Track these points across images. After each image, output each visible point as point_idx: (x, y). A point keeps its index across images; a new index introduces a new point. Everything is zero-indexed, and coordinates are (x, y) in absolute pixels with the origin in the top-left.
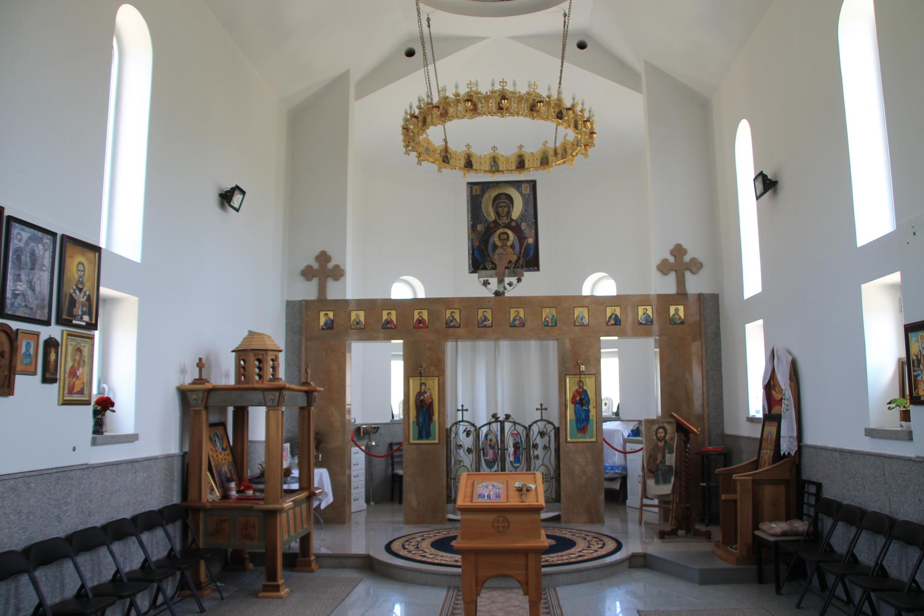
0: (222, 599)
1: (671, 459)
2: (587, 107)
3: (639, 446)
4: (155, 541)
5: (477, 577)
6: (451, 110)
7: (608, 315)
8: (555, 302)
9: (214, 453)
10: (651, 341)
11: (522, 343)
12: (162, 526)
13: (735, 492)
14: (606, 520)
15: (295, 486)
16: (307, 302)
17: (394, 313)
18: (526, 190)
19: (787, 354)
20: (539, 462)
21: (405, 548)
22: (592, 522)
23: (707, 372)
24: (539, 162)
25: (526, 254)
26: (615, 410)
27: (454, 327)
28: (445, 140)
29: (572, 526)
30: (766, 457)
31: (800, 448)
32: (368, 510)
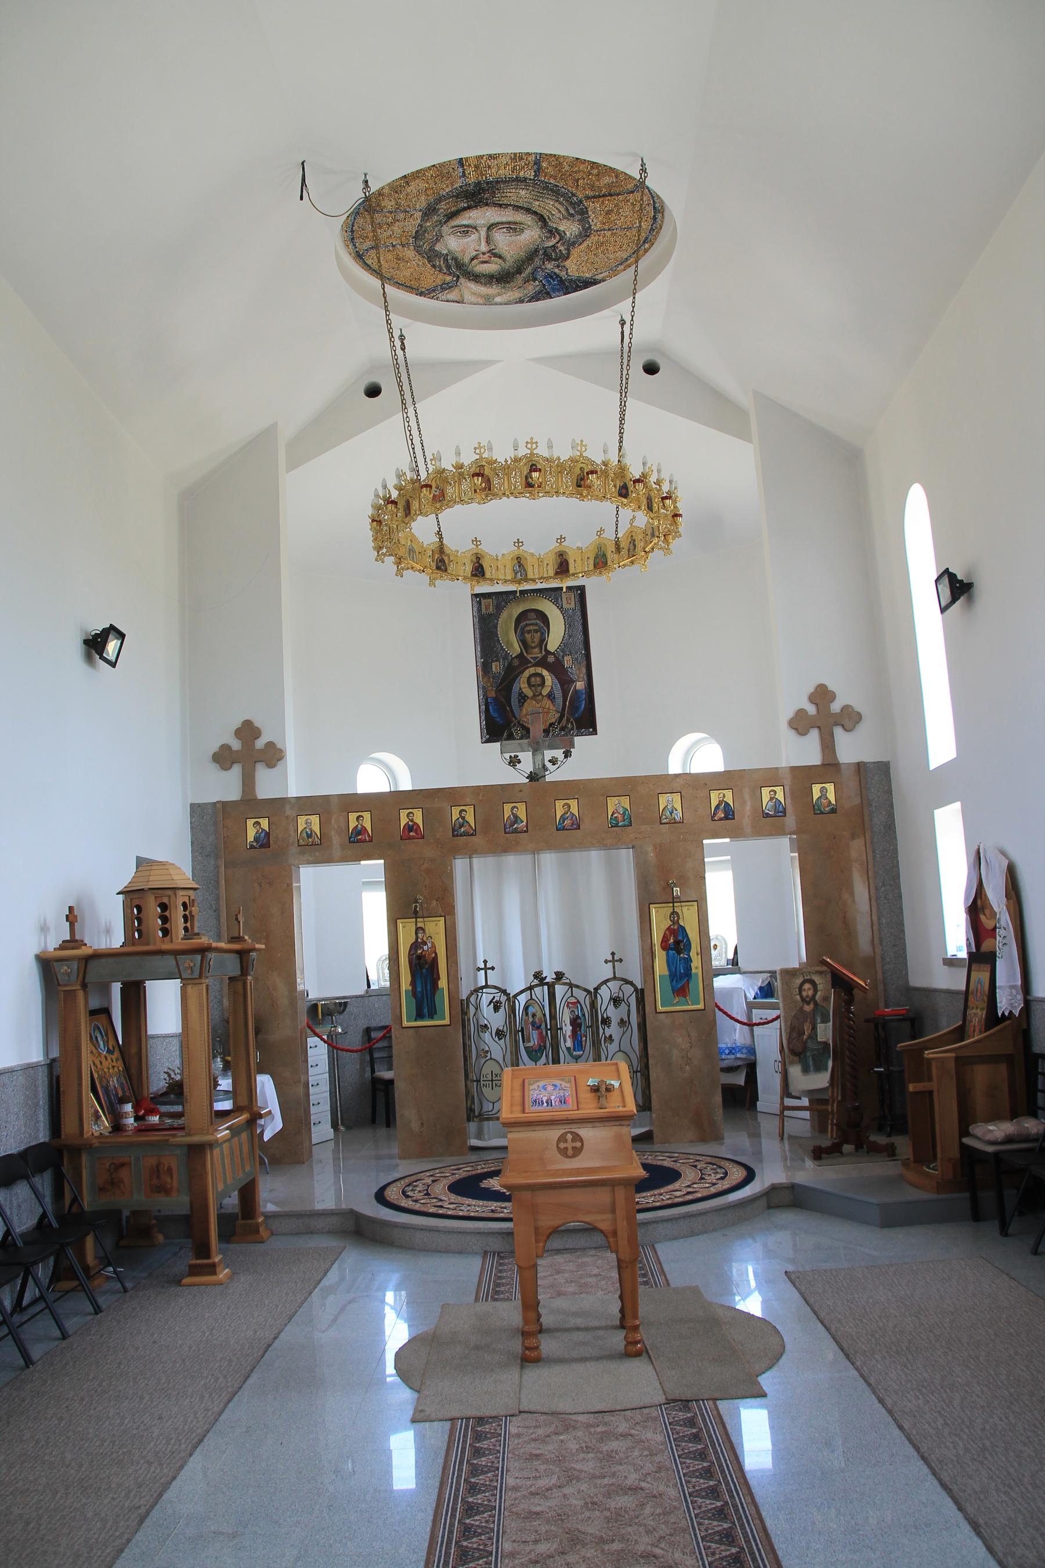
0: (125, 1290)
1: (825, 1032)
2: (665, 476)
3: (774, 1013)
4: (15, 1203)
5: (536, 1229)
6: (450, 491)
7: (714, 803)
8: (627, 786)
9: (95, 1060)
10: (785, 842)
11: (577, 856)
12: (26, 1178)
13: (930, 1079)
14: (726, 1135)
15: (226, 1105)
16: (224, 804)
17: (367, 816)
18: (570, 602)
19: (1001, 856)
20: (613, 1047)
21: (407, 1197)
22: (703, 1140)
23: (877, 889)
24: (591, 562)
25: (574, 706)
26: (731, 956)
27: (466, 834)
28: (439, 533)
29: (672, 1147)
30: (975, 1021)
31: (1027, 1003)
32: (336, 1139)
